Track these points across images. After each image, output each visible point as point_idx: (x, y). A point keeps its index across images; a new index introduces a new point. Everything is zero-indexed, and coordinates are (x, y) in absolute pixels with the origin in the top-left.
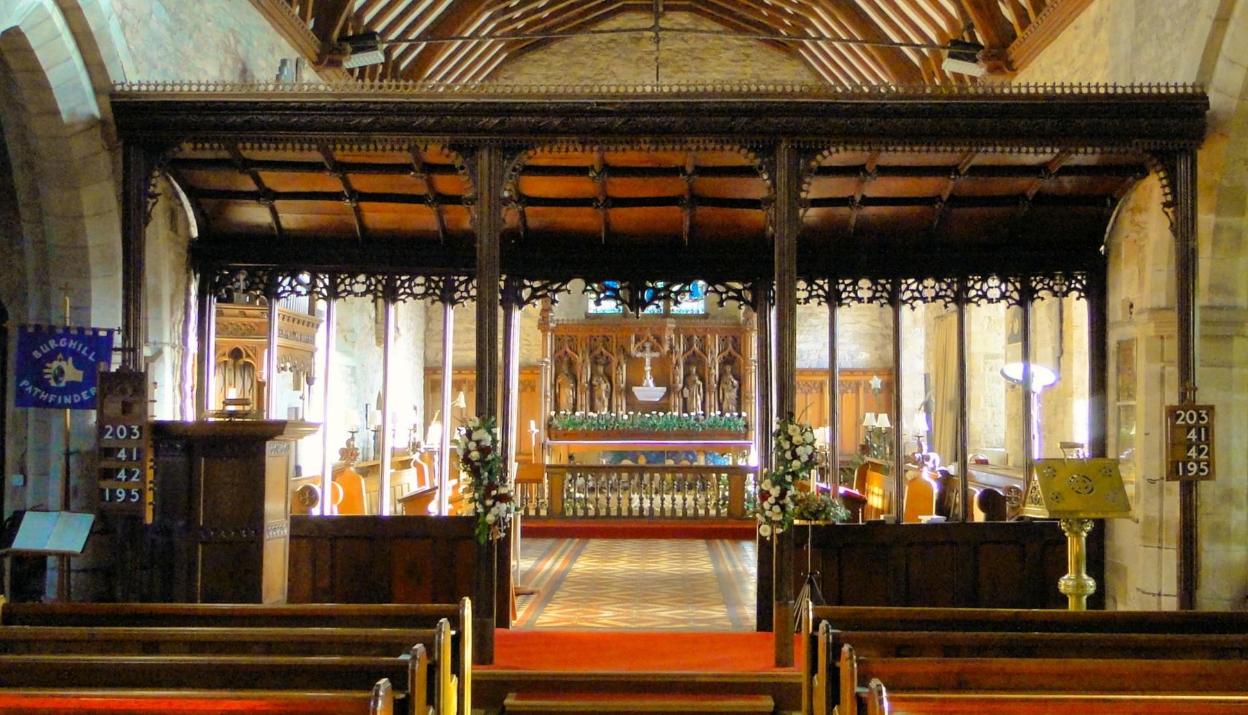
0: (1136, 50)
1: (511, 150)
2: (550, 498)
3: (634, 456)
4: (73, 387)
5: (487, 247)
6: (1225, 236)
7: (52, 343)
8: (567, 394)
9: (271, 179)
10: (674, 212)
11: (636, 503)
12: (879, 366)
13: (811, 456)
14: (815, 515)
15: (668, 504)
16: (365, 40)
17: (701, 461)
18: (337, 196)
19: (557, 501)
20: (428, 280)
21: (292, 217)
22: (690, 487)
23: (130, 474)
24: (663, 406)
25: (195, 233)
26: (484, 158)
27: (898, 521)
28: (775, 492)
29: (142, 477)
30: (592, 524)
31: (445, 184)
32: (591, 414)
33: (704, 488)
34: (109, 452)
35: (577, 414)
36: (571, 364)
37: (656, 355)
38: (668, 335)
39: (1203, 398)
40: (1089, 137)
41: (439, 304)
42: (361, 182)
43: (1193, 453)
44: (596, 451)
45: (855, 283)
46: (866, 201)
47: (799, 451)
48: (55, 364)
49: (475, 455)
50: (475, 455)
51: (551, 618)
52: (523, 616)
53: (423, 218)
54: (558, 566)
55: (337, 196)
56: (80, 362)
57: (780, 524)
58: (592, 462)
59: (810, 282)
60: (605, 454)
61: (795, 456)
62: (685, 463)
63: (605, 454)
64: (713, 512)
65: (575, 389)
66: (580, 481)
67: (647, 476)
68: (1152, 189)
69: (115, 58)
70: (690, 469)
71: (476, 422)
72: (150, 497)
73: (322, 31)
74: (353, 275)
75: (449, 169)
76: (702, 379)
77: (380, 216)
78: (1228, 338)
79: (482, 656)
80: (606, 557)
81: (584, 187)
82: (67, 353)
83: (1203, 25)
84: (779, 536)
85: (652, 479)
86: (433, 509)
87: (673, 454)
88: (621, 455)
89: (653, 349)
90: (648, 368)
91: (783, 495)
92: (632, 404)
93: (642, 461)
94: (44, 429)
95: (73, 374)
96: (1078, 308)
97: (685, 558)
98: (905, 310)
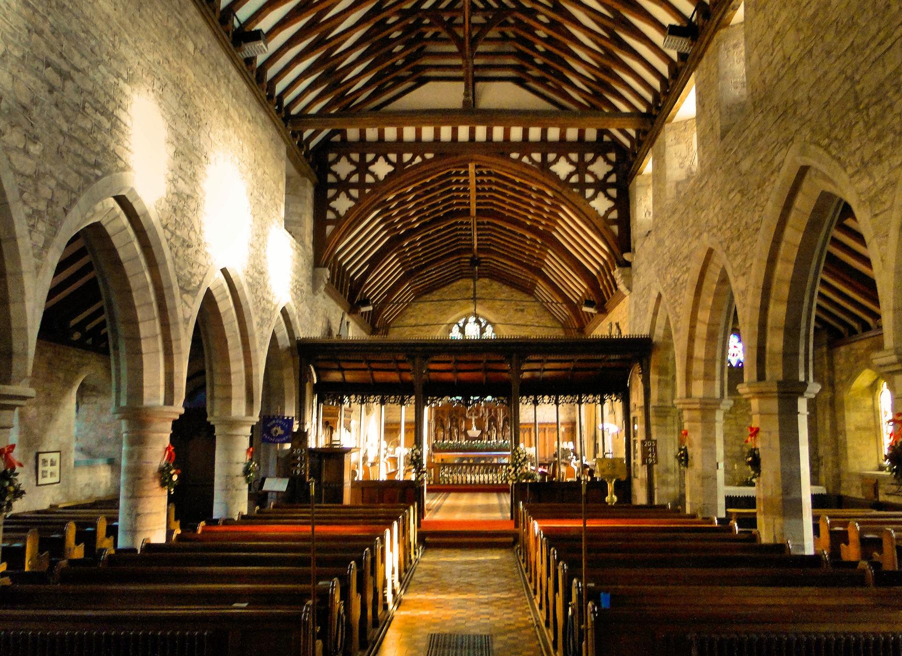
0: (635, 318)
1: (426, 358)
2: (434, 476)
3: (468, 459)
4: (280, 436)
5: (418, 387)
6: (662, 383)
7: (274, 422)
8: (441, 433)
9: (344, 365)
10: (480, 374)
11: (469, 479)
12: (568, 421)
13: (525, 458)
14: (529, 478)
15: (482, 479)
16: (366, 302)
17: (495, 461)
18: (365, 370)
19: (437, 478)
20: (395, 397)
21: (349, 377)
22: (491, 472)
23: (301, 465)
24: (480, 438)
25: (315, 381)
26: (417, 361)
27: (559, 480)
28: (513, 469)
29: (306, 465)
30: (451, 487)
31: (402, 366)
32: (450, 442)
33: (496, 472)
34: (295, 458)
35: (445, 442)
36: (442, 421)
37: (477, 417)
38: (482, 409)
39: (654, 437)
40: (616, 352)
41: (399, 406)
42: (373, 366)
43: (650, 455)
44: (453, 457)
45: (543, 397)
46: (545, 370)
47: (521, 456)
48: (275, 429)
49: (415, 458)
50: (415, 458)
51: (438, 517)
52: (428, 517)
53: (394, 377)
54: (439, 502)
55: (365, 370)
56: (283, 428)
57: (515, 480)
58: (450, 461)
59: (528, 397)
60: (456, 458)
61: (519, 457)
62: (489, 462)
63: (456, 458)
64: (500, 482)
65: (444, 431)
66: (446, 470)
67: (473, 468)
68: (637, 368)
69: (297, 328)
70: (490, 464)
71: (415, 447)
72: (308, 473)
73: (351, 299)
74: (370, 396)
75: (403, 362)
76: (496, 427)
77: (379, 376)
78: (666, 417)
79: (419, 526)
80: (457, 498)
81: (449, 366)
82: (278, 425)
83: (650, 316)
84: (515, 484)
85: (475, 468)
86: (397, 478)
87: (484, 458)
88: (463, 459)
89: (475, 415)
90: (473, 423)
91: (515, 470)
92: (467, 438)
93: (471, 461)
94: (267, 451)
95: (280, 432)
96: (619, 405)
97: (488, 498)
98: (560, 406)
